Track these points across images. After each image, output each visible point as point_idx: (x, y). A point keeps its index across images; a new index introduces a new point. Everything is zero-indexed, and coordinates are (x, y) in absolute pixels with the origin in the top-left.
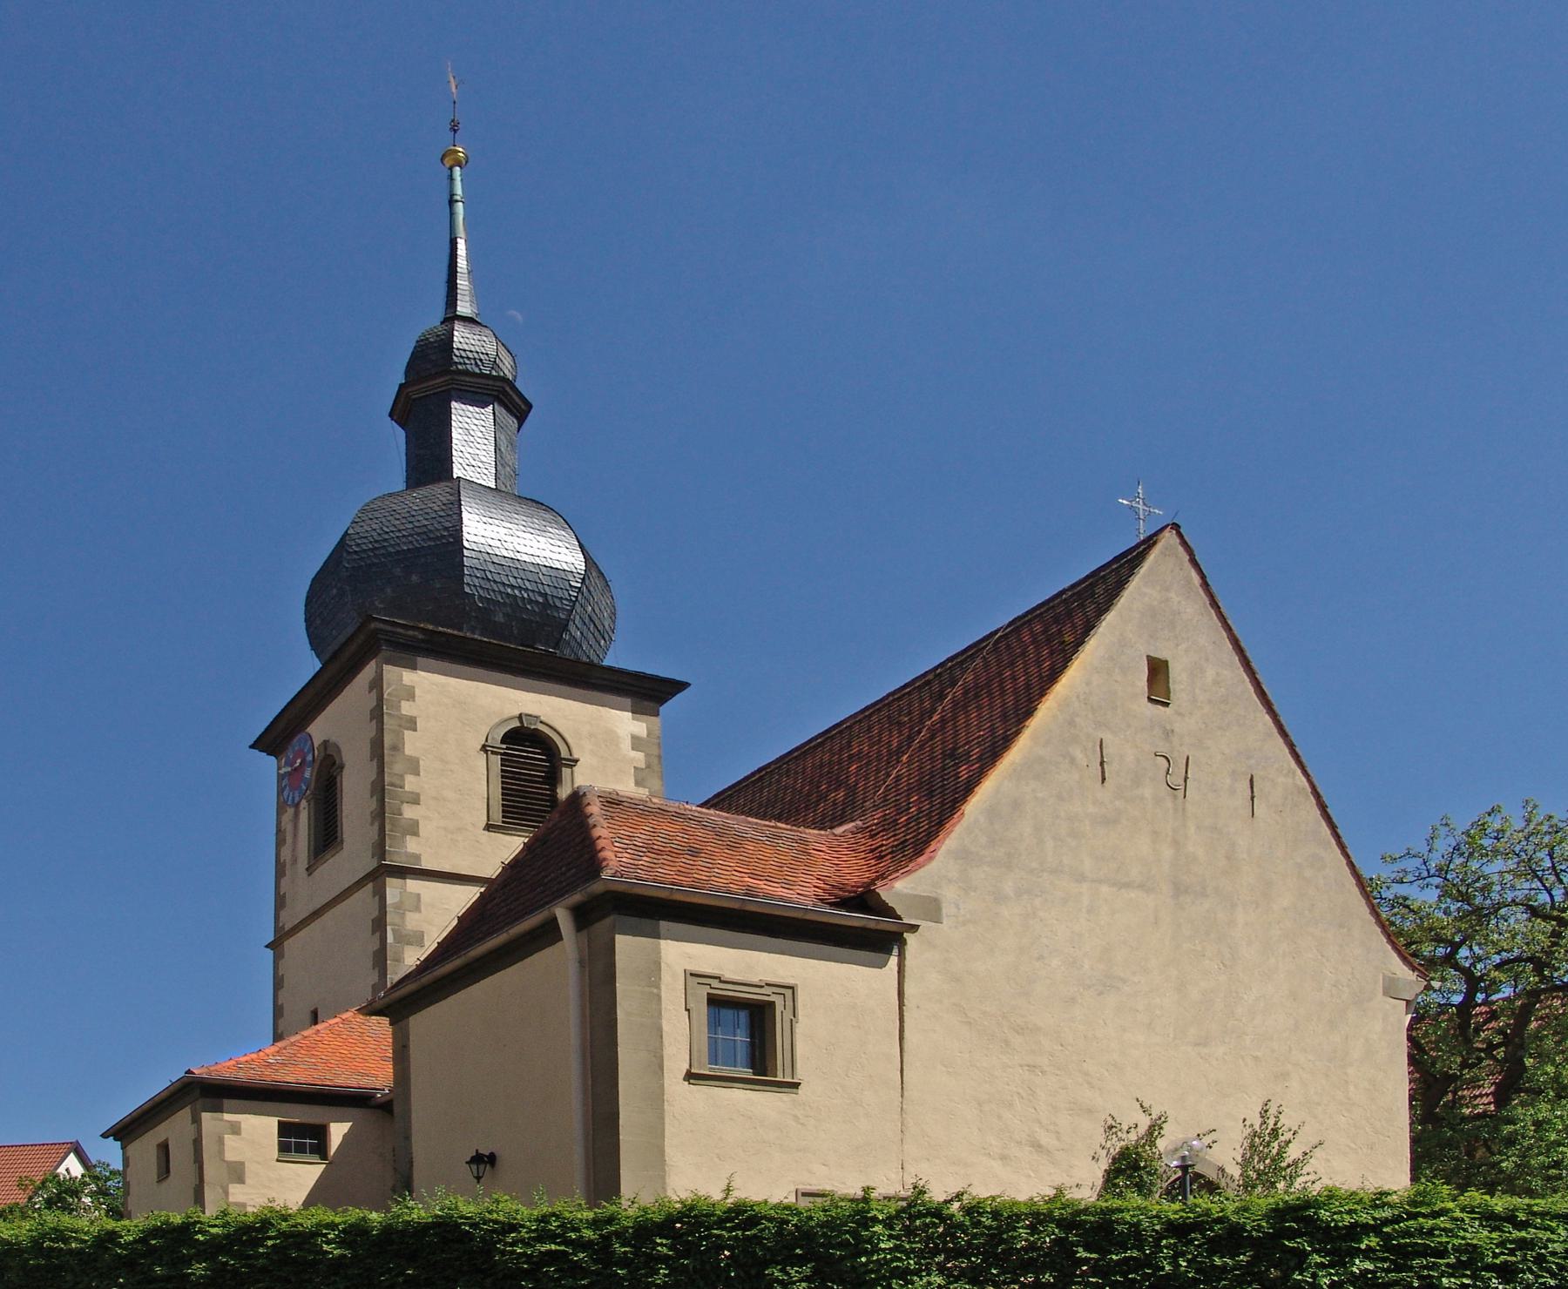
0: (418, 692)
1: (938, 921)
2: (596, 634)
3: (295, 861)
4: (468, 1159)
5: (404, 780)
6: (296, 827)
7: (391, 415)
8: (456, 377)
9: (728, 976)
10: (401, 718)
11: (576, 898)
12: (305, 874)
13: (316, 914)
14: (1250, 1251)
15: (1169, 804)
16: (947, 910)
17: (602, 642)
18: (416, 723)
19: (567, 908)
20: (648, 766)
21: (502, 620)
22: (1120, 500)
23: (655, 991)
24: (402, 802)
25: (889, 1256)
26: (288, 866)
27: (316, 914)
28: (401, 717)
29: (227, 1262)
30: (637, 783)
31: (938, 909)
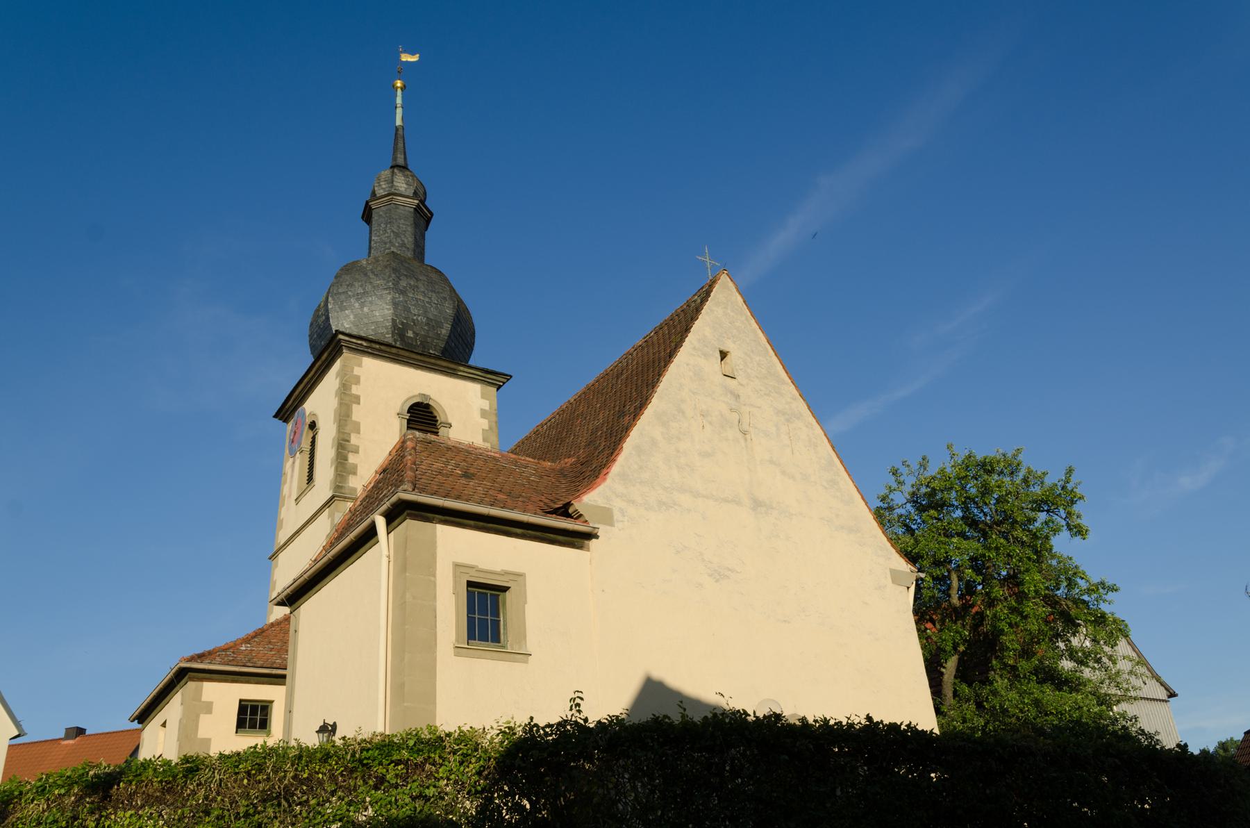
0: (362, 379)
1: (612, 525)
2: (464, 345)
3: (290, 496)
4: (318, 729)
5: (350, 437)
6: (293, 471)
7: (363, 218)
8: (395, 197)
9: (482, 566)
10: (351, 396)
11: (384, 508)
12: (293, 503)
13: (298, 532)
14: (560, 800)
15: (742, 441)
16: (617, 515)
17: (467, 350)
18: (359, 400)
19: (381, 515)
20: (490, 428)
21: (412, 336)
22: (697, 257)
23: (433, 579)
24: (349, 452)
25: (694, 807)
26: (286, 499)
27: (298, 532)
28: (352, 395)
29: (1082, 805)
30: (484, 440)
31: (611, 517)
